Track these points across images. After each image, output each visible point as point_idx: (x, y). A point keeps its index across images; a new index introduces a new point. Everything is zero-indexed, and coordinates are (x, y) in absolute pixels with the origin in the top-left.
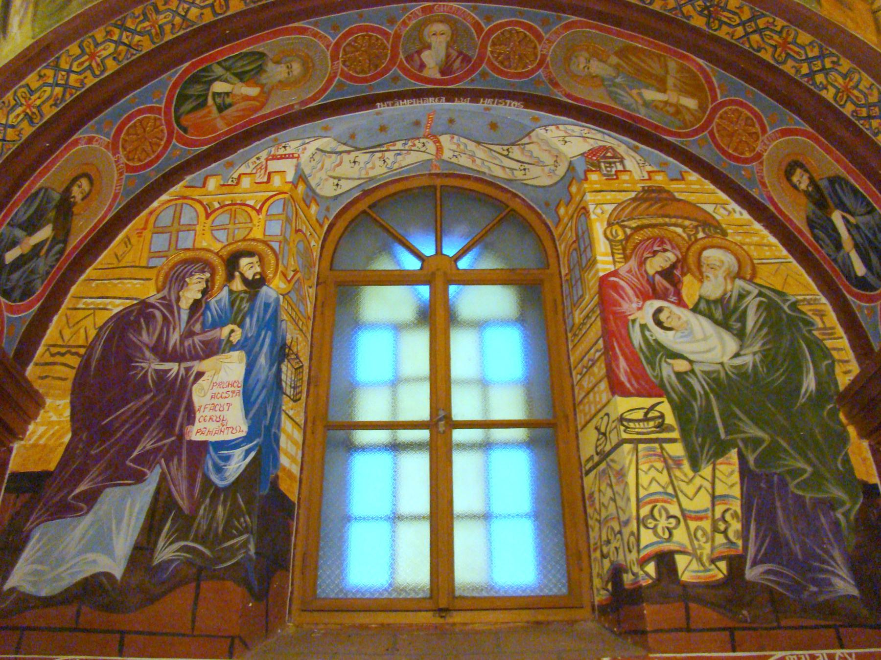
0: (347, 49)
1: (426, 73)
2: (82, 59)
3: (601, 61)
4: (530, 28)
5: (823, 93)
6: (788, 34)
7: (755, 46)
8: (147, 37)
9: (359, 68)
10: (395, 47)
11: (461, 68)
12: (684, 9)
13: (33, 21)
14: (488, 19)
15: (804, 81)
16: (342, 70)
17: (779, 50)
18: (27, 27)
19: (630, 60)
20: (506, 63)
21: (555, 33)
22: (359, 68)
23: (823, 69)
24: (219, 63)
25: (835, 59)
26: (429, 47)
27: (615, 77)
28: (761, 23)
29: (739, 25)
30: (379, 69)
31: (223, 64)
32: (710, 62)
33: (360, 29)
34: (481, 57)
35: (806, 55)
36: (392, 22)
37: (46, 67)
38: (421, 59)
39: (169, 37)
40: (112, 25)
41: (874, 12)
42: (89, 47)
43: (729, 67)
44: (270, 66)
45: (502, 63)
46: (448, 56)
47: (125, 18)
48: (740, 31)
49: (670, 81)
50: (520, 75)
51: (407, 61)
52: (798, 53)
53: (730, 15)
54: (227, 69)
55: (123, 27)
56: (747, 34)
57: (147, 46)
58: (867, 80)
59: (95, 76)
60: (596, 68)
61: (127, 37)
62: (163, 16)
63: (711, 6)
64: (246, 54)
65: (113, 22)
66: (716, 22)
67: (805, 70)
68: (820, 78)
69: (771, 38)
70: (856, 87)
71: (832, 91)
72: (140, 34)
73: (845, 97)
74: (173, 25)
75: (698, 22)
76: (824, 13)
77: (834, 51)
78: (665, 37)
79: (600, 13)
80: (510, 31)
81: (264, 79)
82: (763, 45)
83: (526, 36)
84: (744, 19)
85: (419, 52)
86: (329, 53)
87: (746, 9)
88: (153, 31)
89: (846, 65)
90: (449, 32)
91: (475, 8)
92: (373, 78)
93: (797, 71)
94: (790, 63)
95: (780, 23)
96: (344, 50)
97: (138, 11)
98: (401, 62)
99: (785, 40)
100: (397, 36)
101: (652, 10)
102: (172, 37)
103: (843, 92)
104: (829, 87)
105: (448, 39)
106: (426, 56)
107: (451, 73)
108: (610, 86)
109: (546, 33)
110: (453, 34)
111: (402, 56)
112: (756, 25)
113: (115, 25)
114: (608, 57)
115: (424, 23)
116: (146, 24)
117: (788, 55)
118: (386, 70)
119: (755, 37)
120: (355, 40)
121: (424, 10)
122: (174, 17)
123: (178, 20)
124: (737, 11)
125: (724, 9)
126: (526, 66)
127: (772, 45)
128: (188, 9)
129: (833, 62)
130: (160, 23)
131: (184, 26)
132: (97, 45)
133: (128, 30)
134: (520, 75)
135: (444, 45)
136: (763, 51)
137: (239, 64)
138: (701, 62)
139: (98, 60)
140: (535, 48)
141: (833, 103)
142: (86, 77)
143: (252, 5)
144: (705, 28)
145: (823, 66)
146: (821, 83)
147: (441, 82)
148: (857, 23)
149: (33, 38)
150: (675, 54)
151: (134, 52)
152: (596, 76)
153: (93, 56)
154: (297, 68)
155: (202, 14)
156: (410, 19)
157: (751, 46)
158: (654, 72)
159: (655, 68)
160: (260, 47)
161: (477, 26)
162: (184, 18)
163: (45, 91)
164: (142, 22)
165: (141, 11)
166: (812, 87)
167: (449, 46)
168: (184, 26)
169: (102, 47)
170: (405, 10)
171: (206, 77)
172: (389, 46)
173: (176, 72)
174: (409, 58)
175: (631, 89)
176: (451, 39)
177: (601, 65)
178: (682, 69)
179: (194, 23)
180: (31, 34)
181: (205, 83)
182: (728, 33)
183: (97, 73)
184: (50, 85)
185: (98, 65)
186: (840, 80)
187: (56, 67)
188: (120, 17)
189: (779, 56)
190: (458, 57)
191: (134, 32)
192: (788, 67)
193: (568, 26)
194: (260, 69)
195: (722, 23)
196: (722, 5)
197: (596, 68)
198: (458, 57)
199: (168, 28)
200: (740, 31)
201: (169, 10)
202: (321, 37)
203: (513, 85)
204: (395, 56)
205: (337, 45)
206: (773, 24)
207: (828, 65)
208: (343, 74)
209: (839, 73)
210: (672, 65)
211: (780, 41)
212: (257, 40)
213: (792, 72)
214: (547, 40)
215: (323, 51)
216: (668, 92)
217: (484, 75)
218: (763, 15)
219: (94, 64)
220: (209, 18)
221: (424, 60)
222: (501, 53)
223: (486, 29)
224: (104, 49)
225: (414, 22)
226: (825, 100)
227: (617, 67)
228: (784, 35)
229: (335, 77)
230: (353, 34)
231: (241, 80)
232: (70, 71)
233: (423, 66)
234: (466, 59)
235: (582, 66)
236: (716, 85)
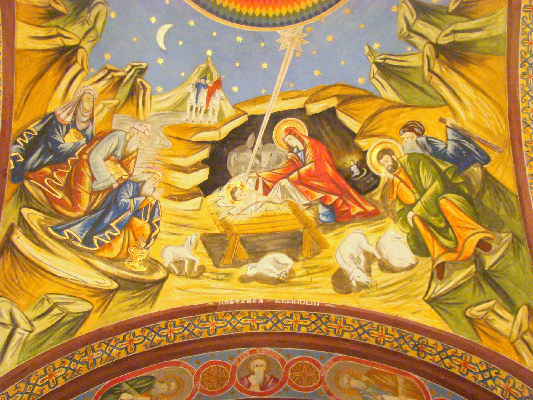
0: (205, 375)
1: (252, 389)
2: (45, 378)
3: (356, 379)
4: (314, 362)
5: (494, 392)
6: (466, 358)
7: (448, 366)
8: (85, 365)
9: (211, 386)
10: (233, 374)
11: (272, 386)
12: (403, 347)
13: (20, 354)
14: (289, 356)
15: (481, 384)
16: (201, 387)
17: (462, 367)
18: (16, 358)
19: (374, 378)
20: (300, 382)
21: (328, 363)
22: (211, 386)
23: (491, 377)
24: (127, 382)
25: (497, 371)
26: (253, 374)
27: (366, 389)
28: (449, 352)
29: (436, 354)
30: (223, 387)
31: (129, 383)
32: (422, 377)
33: (212, 363)
34: (285, 378)
35: (479, 369)
36: (231, 358)
37: (20, 383)
38: (248, 380)
39: (98, 366)
40: (66, 358)
41: (512, 343)
42: (50, 371)
43: (437, 380)
44: (157, 384)
45: (297, 382)
46: (265, 378)
47: (74, 354)
48: (437, 358)
49: (400, 389)
50: (308, 389)
51: (240, 382)
52: (474, 369)
53: (430, 349)
54: (131, 386)
55: (72, 359)
56: (442, 359)
57: (85, 370)
58: (519, 383)
59: (50, 388)
60: (354, 383)
61: (73, 365)
62: (96, 353)
63: (419, 344)
64: (144, 377)
65: (67, 356)
66: (423, 353)
67: (480, 378)
68: (490, 382)
69: (457, 361)
70: (514, 386)
71: (499, 390)
72: (82, 363)
73: (508, 394)
74: (102, 359)
75: (413, 354)
76: (484, 345)
77: (495, 366)
78: (394, 364)
79: (353, 351)
80: (301, 363)
81: (153, 392)
82: (452, 365)
83: (311, 366)
84: (439, 350)
85: (247, 377)
86: (193, 378)
87: (439, 345)
88: (90, 362)
89: (504, 374)
90: (266, 364)
91: (280, 350)
92: (220, 392)
93: (475, 379)
94: (470, 374)
95: (460, 352)
96: (202, 375)
97: (82, 350)
98: (237, 383)
99: (465, 361)
100: (234, 367)
101: (3, 90)
102: (100, 366)
103: (506, 390)
104: (497, 388)
105: (265, 369)
106: (251, 379)
107: (266, 389)
108: (364, 394)
109: (323, 364)
110: (268, 366)
111: (237, 379)
112: (446, 353)
113: (68, 358)
114: (361, 377)
115: (251, 360)
116: (86, 358)
117: (468, 370)
118: (227, 388)
119: (447, 361)
120: (209, 370)
121: (251, 352)
122: (103, 354)
123: (105, 356)
124: (434, 346)
125: (427, 345)
126: (311, 384)
127: (457, 365)
128: (112, 350)
129: (496, 373)
130: (94, 357)
131: (108, 360)
132: (55, 369)
133: (74, 361)
134: (308, 389)
135: (262, 372)
136: (453, 369)
137: (139, 383)
138: (417, 377)
139: (54, 378)
140: (317, 373)
141: (501, 397)
142: (44, 389)
143: (150, 348)
144: (417, 357)
145: (490, 375)
146: (491, 385)
147: (260, 394)
148: (505, 350)
149: (18, 364)
150: (402, 373)
151: (77, 374)
152: (355, 389)
153: (51, 376)
154: (173, 385)
155: (120, 353)
156: (242, 357)
157: (445, 366)
158: (388, 384)
159: (390, 382)
160: (152, 373)
161: (282, 360)
162: (109, 355)
163: (17, 397)
164: (83, 357)
165: (84, 351)
166: (487, 388)
167: (265, 373)
168: (108, 360)
169: (58, 370)
170: (239, 352)
171: (118, 390)
172: (229, 373)
173: (100, 387)
174: (242, 380)
175: (376, 395)
176: (267, 368)
177: (358, 381)
178: (406, 382)
179: (114, 358)
180: (17, 361)
181: (116, 394)
182: (431, 359)
183: (52, 386)
184: (22, 393)
185: (53, 381)
186: (502, 383)
187: (28, 382)
188: (71, 354)
189: (463, 370)
190: (270, 379)
191: (78, 362)
192: (470, 377)
193: (336, 360)
194: (151, 387)
195: (426, 354)
196: (425, 343)
197: (354, 383)
198: (270, 379)
199: (98, 360)
200: (437, 358)
201: (100, 350)
202: (189, 368)
203: (305, 395)
204: (232, 379)
205: (199, 372)
206: (456, 353)
207: (493, 375)
208: (201, 390)
209: (502, 379)
210: (400, 379)
211: (462, 362)
212: (151, 369)
213: (473, 380)
214: (324, 367)
215: (189, 376)
216: (399, 396)
217: (286, 389)
218: (449, 348)
219: (51, 381)
220: (123, 355)
221: (250, 381)
222: (296, 376)
223: (287, 363)
224: (58, 372)
225: (245, 359)
226: (496, 396)
227: (367, 383)
228: (464, 359)
229: (196, 392)
230: (208, 366)
231: (139, 393)
232: (35, 385)
233: (249, 384)
234: (276, 380)
235: (345, 383)
236: (428, 391)
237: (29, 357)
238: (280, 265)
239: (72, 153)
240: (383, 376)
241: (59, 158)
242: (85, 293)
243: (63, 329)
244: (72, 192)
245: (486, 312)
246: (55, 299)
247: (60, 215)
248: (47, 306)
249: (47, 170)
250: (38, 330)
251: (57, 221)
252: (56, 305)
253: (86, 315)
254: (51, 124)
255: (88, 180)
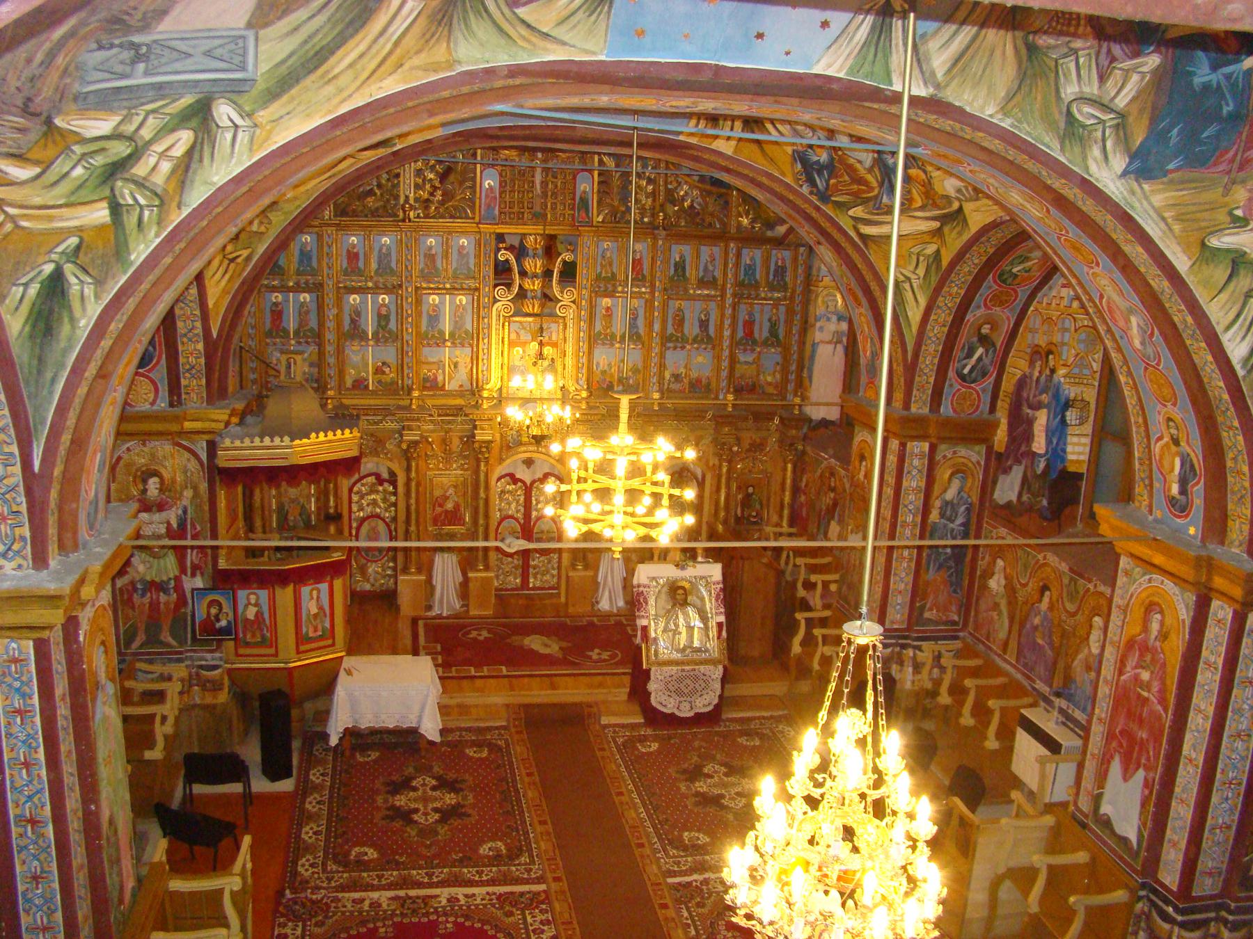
237: (930, 292)
238: (175, 53)
239: (832, 159)
240: (227, 276)
241: (830, 167)
242: (926, 238)
243: (934, 267)
244: (861, 181)
245: (910, 348)
246: (916, 250)
247: (869, 199)
248: (914, 258)
249: (832, 181)
250: (922, 275)
251: (871, 203)
252: (918, 255)
253: (938, 251)
254: (800, 157)
255: (858, 165)
